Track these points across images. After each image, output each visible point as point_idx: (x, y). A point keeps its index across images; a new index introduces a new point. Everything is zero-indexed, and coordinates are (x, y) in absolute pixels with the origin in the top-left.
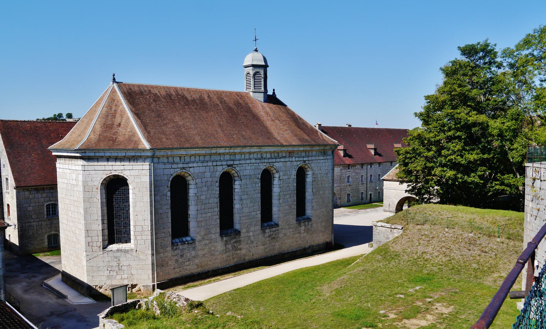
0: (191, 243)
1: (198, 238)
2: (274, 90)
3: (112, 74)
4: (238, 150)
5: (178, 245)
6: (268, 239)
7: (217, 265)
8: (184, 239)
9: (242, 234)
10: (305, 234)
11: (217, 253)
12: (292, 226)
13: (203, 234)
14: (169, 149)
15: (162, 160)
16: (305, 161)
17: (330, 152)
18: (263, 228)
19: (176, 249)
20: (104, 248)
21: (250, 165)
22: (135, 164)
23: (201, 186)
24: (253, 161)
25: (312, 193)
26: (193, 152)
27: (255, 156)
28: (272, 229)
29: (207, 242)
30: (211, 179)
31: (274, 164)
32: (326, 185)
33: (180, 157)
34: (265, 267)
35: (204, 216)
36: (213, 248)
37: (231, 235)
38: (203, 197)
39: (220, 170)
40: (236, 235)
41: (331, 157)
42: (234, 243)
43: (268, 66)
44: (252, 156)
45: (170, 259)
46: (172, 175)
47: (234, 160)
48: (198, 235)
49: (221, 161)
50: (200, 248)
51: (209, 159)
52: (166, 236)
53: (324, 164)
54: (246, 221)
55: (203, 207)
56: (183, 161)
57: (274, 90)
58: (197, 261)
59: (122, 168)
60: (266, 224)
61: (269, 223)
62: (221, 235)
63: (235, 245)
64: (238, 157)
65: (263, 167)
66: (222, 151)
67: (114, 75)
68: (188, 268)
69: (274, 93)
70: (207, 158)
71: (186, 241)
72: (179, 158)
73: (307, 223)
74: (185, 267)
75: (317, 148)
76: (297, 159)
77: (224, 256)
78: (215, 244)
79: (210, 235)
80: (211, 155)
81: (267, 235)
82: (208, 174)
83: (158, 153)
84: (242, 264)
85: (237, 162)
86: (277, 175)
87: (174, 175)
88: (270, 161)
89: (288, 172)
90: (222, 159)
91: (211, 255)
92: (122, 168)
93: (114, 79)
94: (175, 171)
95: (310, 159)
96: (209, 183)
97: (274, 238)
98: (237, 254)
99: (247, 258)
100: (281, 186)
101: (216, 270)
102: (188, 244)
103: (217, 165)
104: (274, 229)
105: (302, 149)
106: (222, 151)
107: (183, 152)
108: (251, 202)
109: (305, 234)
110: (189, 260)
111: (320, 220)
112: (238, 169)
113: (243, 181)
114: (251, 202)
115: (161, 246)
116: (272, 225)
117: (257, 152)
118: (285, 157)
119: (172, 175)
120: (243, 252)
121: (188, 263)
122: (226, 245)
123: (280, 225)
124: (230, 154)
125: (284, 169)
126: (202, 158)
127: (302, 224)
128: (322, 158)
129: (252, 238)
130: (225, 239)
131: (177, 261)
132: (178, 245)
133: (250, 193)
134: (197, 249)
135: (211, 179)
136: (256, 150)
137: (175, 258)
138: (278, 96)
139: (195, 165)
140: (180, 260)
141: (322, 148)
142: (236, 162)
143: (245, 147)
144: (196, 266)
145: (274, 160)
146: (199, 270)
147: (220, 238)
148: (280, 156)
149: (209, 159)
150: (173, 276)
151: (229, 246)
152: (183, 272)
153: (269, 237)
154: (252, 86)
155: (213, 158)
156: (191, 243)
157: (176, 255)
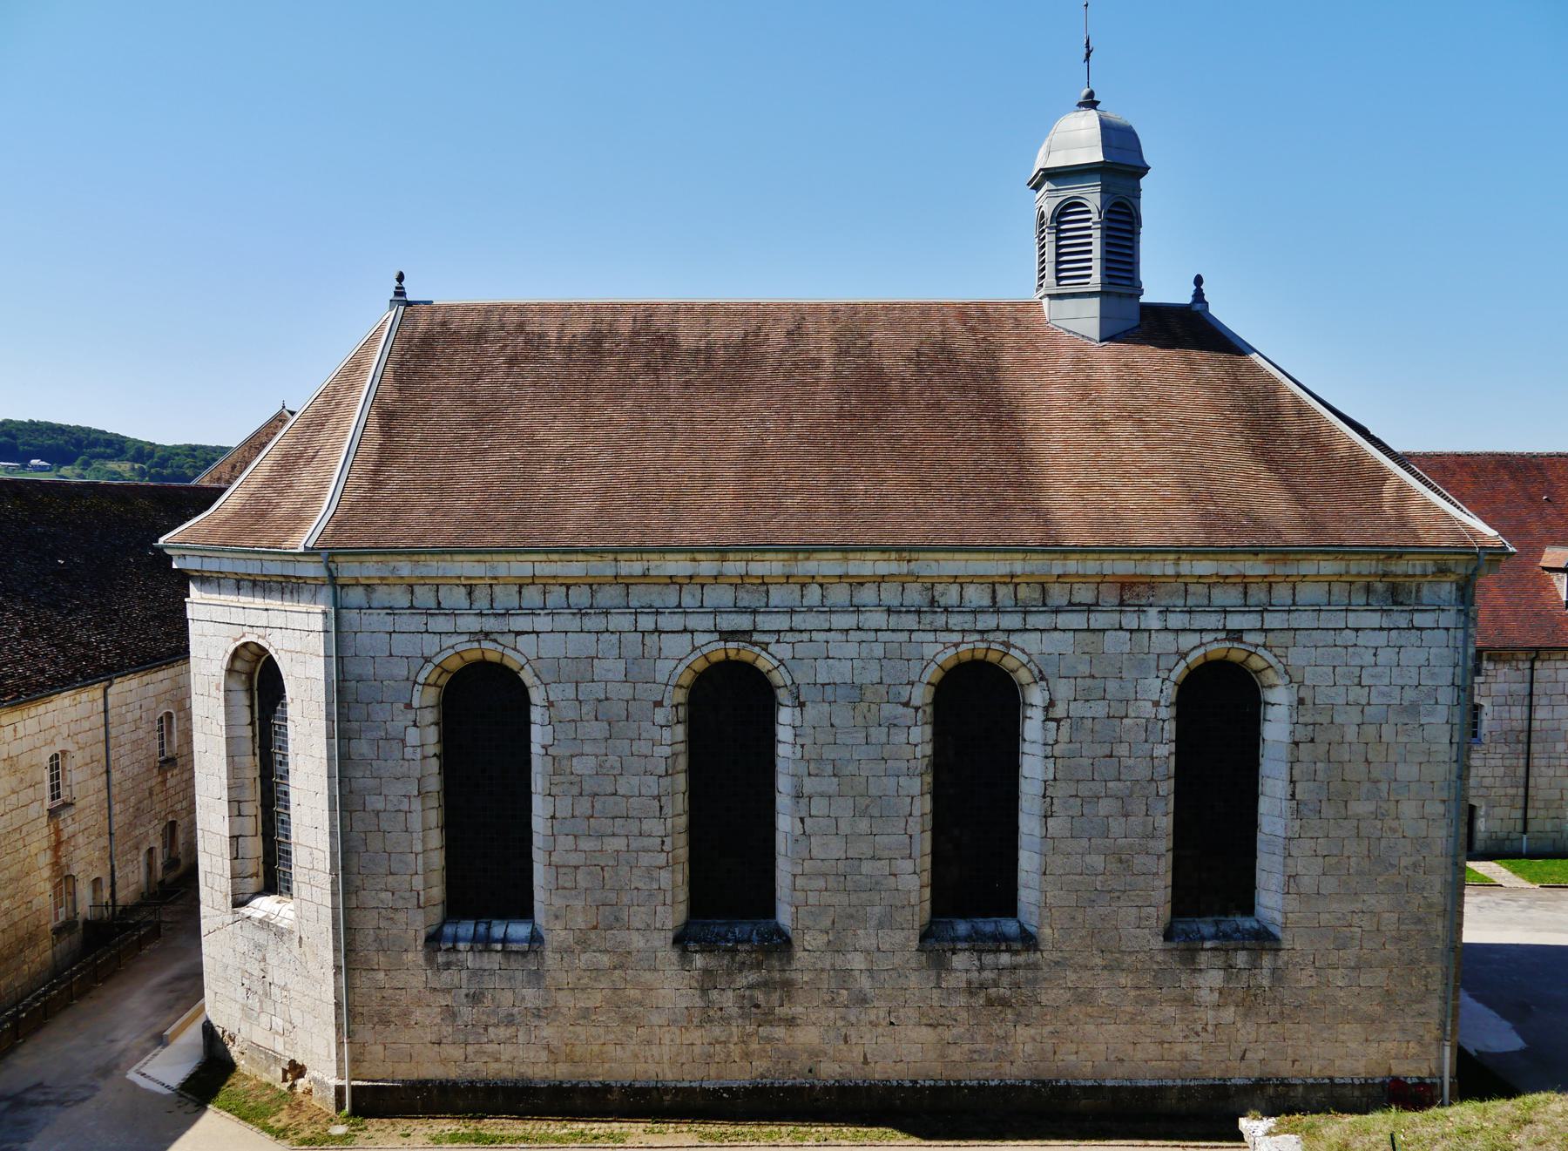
0: (524, 954)
1: (556, 935)
2: (1198, 281)
3: (395, 275)
4: (771, 566)
5: (454, 950)
6: (962, 1000)
7: (652, 1069)
8: (498, 930)
9: (800, 954)
10: (1228, 1014)
11: (656, 1019)
12: (1129, 960)
13: (580, 922)
14: (410, 553)
15: (381, 596)
16: (1236, 635)
17: (1447, 590)
18: (934, 940)
19: (448, 966)
20: (238, 903)
21: (853, 636)
22: (288, 605)
23: (572, 715)
24: (877, 619)
25: (1286, 805)
26: (521, 567)
27: (890, 595)
28: (988, 959)
29: (605, 960)
30: (627, 691)
31: (1015, 639)
32: (1406, 772)
33: (470, 590)
34: (876, 1131)
35: (585, 844)
36: (633, 993)
37: (734, 951)
38: (579, 766)
39: (680, 656)
40: (768, 953)
41: (1449, 618)
42: (750, 987)
43: (1145, 170)
44: (867, 595)
45: (419, 1001)
46: (427, 660)
47: (755, 612)
48: (558, 925)
49: (681, 610)
50: (563, 978)
51: (620, 601)
52: (400, 904)
53: (1386, 656)
54: (827, 898)
55: (584, 806)
56: (482, 603)
57: (1198, 281)
58: (547, 1032)
59: (263, 619)
60: (962, 927)
61: (987, 926)
62: (681, 940)
63: (760, 996)
64: (778, 596)
65: (939, 651)
66: (677, 566)
67: (401, 278)
68: (507, 1052)
69: (1199, 295)
70: (608, 596)
71: (505, 940)
72: (463, 590)
73: (1241, 959)
74: (490, 1048)
75: (1329, 567)
76: (1175, 621)
77: (696, 1035)
78: (648, 976)
79: (622, 935)
80: (626, 583)
81: (950, 981)
82: (612, 668)
83: (349, 569)
84: (795, 1091)
85: (782, 622)
86: (1036, 695)
87: (1195, 657)
88: (987, 621)
89: (1112, 686)
90: (687, 600)
91: (625, 1020)
92: (263, 619)
93: (400, 292)
94: (453, 642)
95: (1272, 621)
96: (618, 709)
97: (1004, 1003)
98: (769, 1040)
99: (829, 1071)
100: (1058, 750)
101: (644, 1092)
102: (506, 952)
103: (963, 631)
104: (1005, 959)
105: (1204, 567)
106: (677, 566)
107: (467, 567)
108: (859, 813)
109: (1228, 1014)
110: (510, 1021)
111: (1350, 955)
112: (783, 651)
113: (809, 708)
114: (859, 813)
115: (377, 939)
116: (1005, 938)
117: (903, 581)
118: (1089, 608)
119: (427, 660)
120: (807, 1036)
121: (503, 1032)
122: (704, 991)
123: (1046, 945)
124: (741, 582)
125: (1084, 669)
126: (580, 597)
127: (1203, 958)
128: (1374, 620)
129: (865, 983)
130: (699, 961)
131: (450, 1014)
132: (454, 950)
133: (852, 768)
134: (548, 981)
135: (627, 691)
136: (883, 568)
137: (444, 1000)
138: (1221, 310)
139: (542, 623)
140: (467, 1013)
141: (1367, 566)
142: (764, 622)
143: (811, 550)
144: (544, 1055)
145: (1013, 621)
146: (562, 1072)
147: (674, 956)
148: (1058, 596)
149: (620, 601)
150: (431, 1070)
151: (728, 1000)
152: (478, 1065)
153: (971, 990)
154: (1050, 278)
155: (639, 596)
156: (524, 954)
157: (447, 991)
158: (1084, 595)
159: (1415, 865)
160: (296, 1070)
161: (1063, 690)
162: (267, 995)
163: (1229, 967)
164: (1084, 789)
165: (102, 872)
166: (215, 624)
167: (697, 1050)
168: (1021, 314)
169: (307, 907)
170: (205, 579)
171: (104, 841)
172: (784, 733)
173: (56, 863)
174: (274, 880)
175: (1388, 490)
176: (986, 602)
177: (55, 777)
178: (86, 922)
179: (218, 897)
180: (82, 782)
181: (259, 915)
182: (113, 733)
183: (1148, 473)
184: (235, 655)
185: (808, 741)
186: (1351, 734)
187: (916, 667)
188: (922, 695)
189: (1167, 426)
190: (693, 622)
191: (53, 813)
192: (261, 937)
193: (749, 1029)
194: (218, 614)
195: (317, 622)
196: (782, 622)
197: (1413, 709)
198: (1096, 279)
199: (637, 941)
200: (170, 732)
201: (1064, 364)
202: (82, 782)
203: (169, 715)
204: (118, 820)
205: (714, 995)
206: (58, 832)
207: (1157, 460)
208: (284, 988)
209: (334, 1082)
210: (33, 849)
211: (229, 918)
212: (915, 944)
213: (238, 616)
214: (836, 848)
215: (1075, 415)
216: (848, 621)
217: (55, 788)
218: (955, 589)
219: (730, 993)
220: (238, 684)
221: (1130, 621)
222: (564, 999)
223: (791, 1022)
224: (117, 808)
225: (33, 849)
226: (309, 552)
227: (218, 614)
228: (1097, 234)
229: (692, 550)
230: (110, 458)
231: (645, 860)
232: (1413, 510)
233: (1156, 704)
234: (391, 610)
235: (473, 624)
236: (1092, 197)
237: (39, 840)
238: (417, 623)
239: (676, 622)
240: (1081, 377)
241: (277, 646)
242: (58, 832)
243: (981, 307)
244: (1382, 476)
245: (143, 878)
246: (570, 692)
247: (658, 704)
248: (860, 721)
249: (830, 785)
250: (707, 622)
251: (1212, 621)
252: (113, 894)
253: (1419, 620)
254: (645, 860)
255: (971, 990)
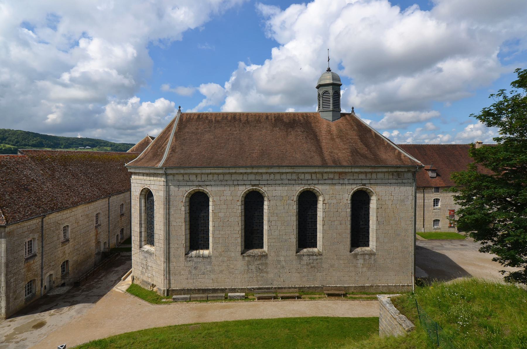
2: (353, 108)
6: (305, 267)
10: (365, 269)
16: (364, 185)
24: (287, 182)
30: (231, 198)
36: (232, 266)
67: (180, 107)
69: (353, 111)
76: (351, 182)
77: (245, 276)
85: (265, 182)
93: (180, 110)
97: (314, 267)
98: (263, 277)
109: (365, 269)
110: (204, 274)
113: (271, 202)
118: (332, 179)
120: (271, 276)
122: (248, 266)
128: (394, 181)
131: (190, 272)
135: (231, 198)
142: (261, 182)
144: (211, 281)
147: (241, 257)
151: (253, 267)
153: (307, 265)
158: (331, 176)
159: (405, 236)
160: (153, 286)
161: (327, 197)
162: (147, 268)
163: (364, 259)
164: (331, 219)
165: (107, 241)
166: (138, 184)
167: (246, 279)
168: (314, 116)
169: (157, 249)
170: (135, 174)
171: (107, 233)
172: (265, 207)
173: (96, 239)
174: (151, 242)
175: (397, 152)
176: (310, 178)
177: (97, 219)
178: (103, 252)
179: (136, 246)
180: (103, 219)
181: (146, 250)
182: (110, 208)
183: (344, 150)
184: (142, 191)
185: (271, 209)
186: (390, 207)
187: (295, 192)
188: (295, 198)
189: (348, 139)
190: (246, 183)
191: (96, 227)
192: (146, 255)
193: (258, 274)
194: (139, 181)
195: (162, 183)
196: (265, 182)
197: (403, 201)
198: (331, 107)
199: (233, 254)
200: (123, 208)
201: (325, 126)
202: (103, 219)
203: (123, 204)
204: (111, 228)
205: (250, 266)
206: (97, 231)
207: (346, 147)
208: (151, 267)
209: (162, 289)
210: (91, 236)
211: (139, 251)
212: (295, 254)
213: (143, 182)
214: (277, 233)
215: (328, 137)
216: (280, 182)
217: (97, 221)
218: (303, 175)
219: (254, 266)
220: (143, 197)
221: (341, 182)
222: (216, 268)
223: (267, 273)
224: (110, 226)
225: (91, 236)
226: (161, 168)
227: (139, 181)
228: (331, 98)
229: (246, 167)
230: (105, 146)
231: (235, 236)
232: (402, 157)
233: (347, 200)
234: (179, 181)
235: (197, 183)
236: (330, 89)
237: (93, 234)
238: (185, 183)
239: (242, 183)
240: (329, 129)
241: (152, 188)
242: (97, 231)
243: (306, 114)
244: (396, 149)
245: (116, 242)
246: (218, 198)
247: (238, 201)
248: (282, 204)
249: (276, 218)
250: (249, 183)
251: (359, 182)
252: (109, 246)
253: (404, 181)
254: (235, 236)
255: (307, 265)
